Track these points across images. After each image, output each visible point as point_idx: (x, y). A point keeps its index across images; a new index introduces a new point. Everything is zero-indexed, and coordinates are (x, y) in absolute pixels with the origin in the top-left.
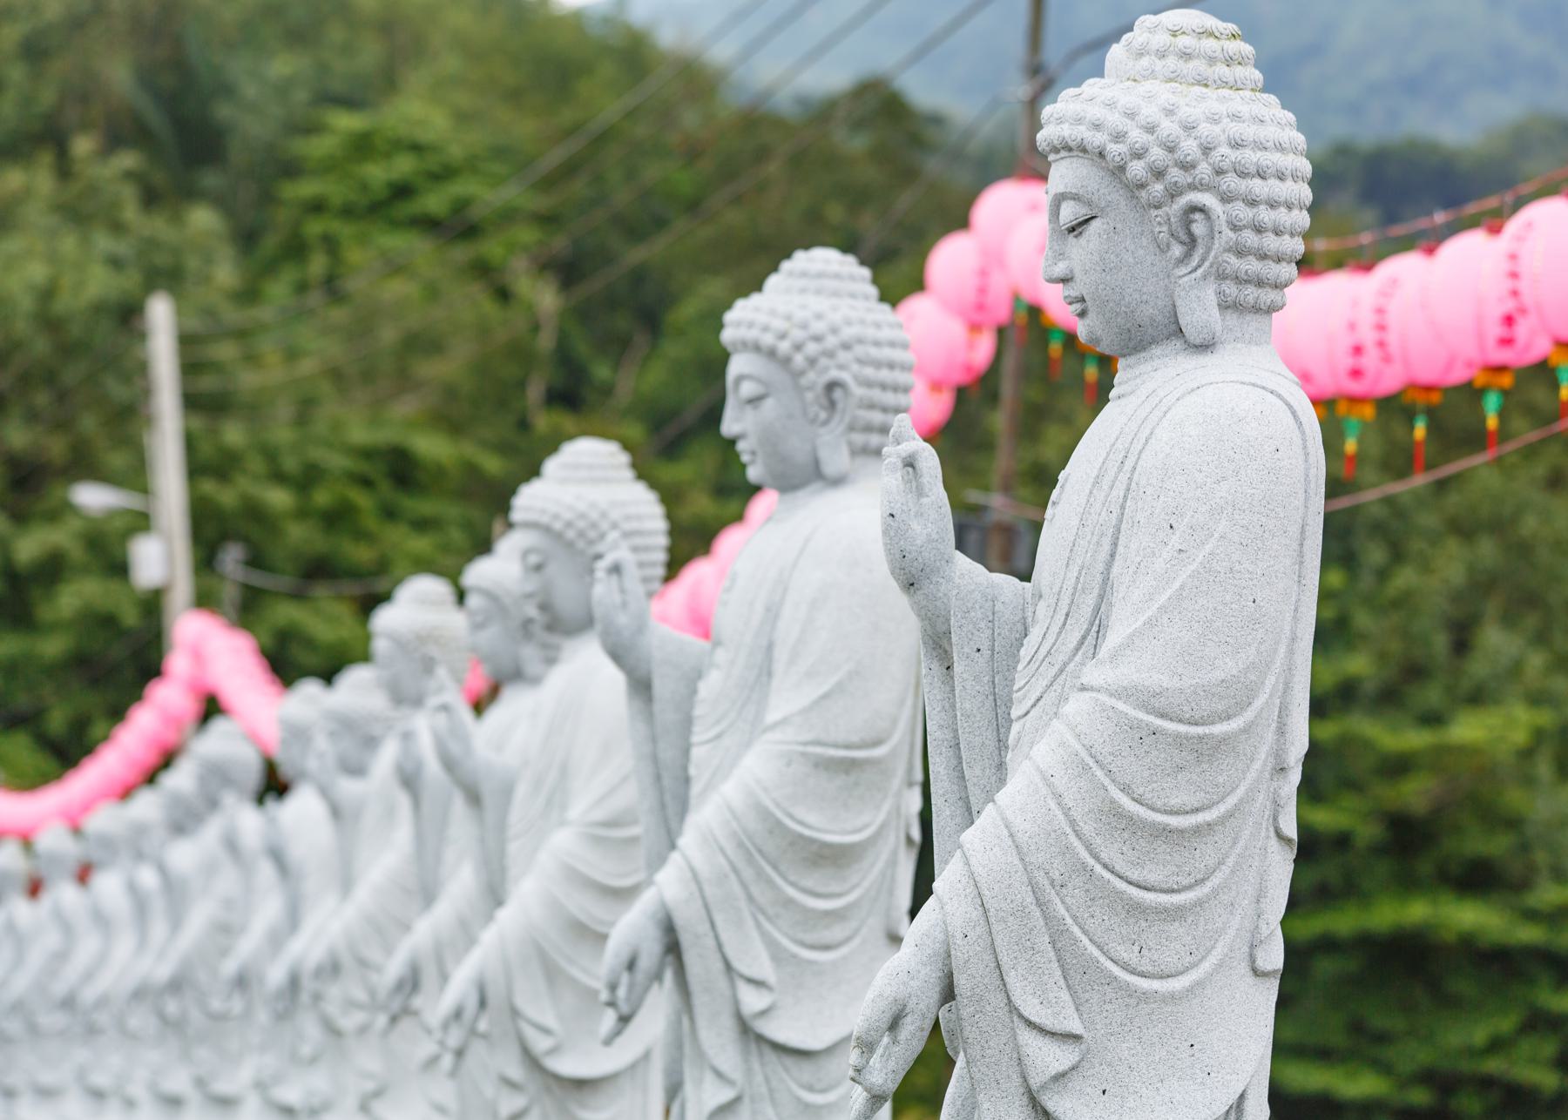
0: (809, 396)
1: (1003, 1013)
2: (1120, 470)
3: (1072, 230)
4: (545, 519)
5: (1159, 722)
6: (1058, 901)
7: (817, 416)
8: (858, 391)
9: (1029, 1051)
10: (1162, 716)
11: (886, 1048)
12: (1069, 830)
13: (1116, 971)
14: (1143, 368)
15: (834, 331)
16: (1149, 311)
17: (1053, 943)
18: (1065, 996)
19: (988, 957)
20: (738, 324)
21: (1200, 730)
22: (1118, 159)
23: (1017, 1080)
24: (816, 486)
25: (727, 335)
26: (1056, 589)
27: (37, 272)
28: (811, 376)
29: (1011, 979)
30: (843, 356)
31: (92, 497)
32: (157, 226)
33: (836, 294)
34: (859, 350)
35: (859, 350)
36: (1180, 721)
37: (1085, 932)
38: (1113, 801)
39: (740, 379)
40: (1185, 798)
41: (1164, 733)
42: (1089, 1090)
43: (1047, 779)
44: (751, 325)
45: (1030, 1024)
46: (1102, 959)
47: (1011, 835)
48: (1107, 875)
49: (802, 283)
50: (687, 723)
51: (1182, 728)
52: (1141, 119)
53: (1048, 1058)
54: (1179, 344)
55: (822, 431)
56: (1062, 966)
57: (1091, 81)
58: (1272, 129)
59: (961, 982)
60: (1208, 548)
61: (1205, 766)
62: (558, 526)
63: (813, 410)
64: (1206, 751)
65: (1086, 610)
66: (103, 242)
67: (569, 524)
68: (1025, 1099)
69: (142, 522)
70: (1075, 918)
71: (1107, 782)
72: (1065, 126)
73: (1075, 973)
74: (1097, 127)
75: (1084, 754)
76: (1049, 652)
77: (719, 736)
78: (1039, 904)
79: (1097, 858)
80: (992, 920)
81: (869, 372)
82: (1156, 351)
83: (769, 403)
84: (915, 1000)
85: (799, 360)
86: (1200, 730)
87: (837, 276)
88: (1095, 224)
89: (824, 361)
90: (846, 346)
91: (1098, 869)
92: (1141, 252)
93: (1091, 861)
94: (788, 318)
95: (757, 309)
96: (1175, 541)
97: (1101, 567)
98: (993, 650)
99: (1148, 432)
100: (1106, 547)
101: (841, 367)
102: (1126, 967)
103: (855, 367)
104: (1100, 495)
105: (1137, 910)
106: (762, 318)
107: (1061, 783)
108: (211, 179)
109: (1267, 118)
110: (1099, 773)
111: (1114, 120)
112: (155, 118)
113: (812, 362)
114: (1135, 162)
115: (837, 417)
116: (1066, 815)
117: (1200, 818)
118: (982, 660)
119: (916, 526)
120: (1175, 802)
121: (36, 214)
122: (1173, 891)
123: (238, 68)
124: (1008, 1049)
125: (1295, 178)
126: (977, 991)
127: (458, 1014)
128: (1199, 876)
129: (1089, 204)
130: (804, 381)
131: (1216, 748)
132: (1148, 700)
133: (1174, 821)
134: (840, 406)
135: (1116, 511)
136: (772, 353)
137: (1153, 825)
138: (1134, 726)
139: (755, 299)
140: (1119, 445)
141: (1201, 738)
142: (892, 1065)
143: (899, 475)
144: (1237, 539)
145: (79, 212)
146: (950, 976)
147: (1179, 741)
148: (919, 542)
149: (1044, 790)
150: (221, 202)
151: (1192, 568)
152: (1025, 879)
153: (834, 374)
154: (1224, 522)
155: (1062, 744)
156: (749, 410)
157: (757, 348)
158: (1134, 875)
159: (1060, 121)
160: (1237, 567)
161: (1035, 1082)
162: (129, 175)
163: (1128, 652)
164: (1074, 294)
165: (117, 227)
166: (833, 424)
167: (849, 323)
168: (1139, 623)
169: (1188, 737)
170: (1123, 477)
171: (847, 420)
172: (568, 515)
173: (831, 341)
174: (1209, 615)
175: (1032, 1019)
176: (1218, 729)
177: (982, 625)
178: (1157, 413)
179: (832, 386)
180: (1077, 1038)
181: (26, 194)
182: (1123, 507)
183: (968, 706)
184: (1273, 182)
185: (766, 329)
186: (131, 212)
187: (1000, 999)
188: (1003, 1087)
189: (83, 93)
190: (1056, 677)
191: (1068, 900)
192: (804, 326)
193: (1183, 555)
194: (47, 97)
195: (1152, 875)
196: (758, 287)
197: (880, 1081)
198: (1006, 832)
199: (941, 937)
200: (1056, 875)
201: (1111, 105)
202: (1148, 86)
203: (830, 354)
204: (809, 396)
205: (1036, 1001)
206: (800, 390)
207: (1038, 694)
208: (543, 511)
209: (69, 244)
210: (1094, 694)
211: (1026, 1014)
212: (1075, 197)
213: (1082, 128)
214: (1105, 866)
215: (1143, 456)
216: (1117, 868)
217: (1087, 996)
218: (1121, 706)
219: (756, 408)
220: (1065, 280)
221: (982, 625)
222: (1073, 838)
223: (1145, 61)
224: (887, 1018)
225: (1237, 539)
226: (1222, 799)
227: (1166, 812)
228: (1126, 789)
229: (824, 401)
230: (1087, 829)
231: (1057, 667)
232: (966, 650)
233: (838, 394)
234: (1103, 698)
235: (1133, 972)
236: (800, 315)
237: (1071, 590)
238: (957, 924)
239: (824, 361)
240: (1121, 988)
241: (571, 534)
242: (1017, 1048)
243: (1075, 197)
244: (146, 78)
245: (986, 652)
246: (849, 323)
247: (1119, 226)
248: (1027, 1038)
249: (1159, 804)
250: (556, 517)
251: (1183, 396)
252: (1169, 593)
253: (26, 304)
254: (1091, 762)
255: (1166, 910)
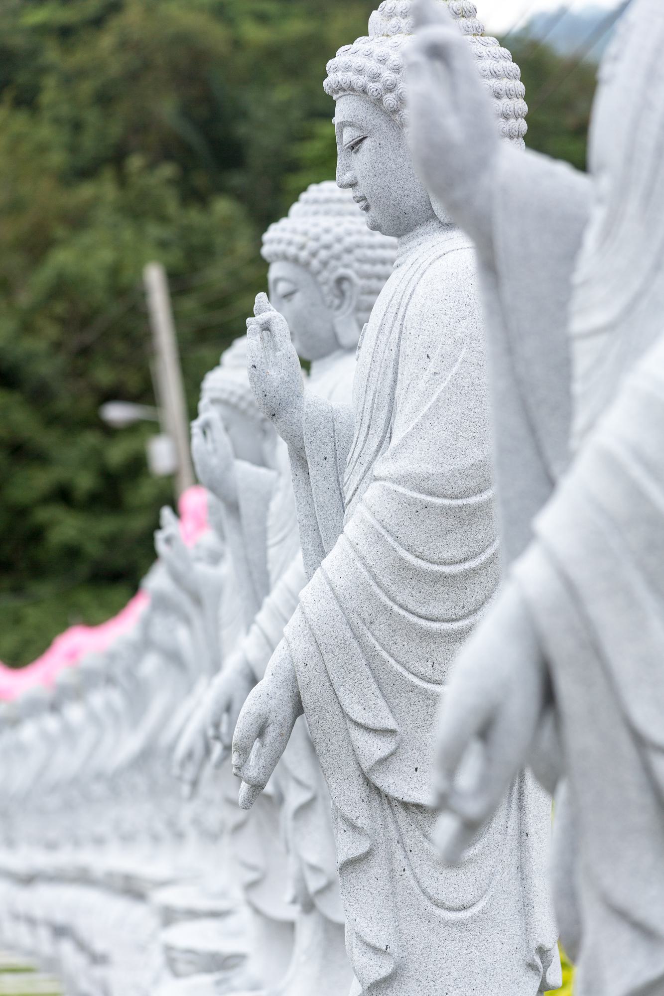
0: (325, 289)
1: (338, 718)
2: (395, 319)
3: (352, 148)
4: (224, 396)
5: (429, 499)
6: (369, 634)
7: (332, 302)
8: (360, 282)
9: (359, 744)
10: (431, 494)
11: (258, 750)
12: (372, 583)
13: (416, 681)
14: (414, 243)
15: (339, 240)
16: (411, 202)
17: (369, 665)
18: (381, 702)
19: (323, 679)
20: (272, 241)
21: (459, 502)
22: (375, 93)
23: (353, 766)
24: (338, 353)
25: (266, 251)
26: (360, 409)
27: (106, 256)
28: (325, 274)
29: (341, 693)
30: (347, 258)
31: (117, 413)
32: (194, 216)
33: (340, 214)
34: (358, 253)
35: (358, 253)
36: (445, 497)
37: (391, 655)
38: (401, 559)
39: (277, 280)
40: (454, 552)
41: (433, 506)
42: (405, 769)
43: (354, 547)
44: (280, 241)
45: (358, 725)
46: (405, 673)
47: (332, 589)
48: (403, 612)
49: (314, 208)
50: (263, 534)
51: (446, 502)
52: (389, 63)
53: (374, 748)
54: (435, 224)
55: (337, 313)
56: (377, 681)
57: (358, 40)
58: (489, 62)
59: (306, 698)
60: (455, 370)
61: (467, 528)
62: (234, 400)
63: (329, 299)
64: (467, 517)
65: (381, 423)
66: (154, 231)
67: (242, 398)
68: (361, 780)
69: (155, 427)
70: (383, 645)
71: (396, 545)
72: (339, 73)
73: (388, 685)
74: (360, 71)
75: (378, 527)
76: (359, 456)
77: (283, 539)
78: (356, 637)
79: (394, 601)
80: (324, 652)
81: (367, 268)
82: (420, 230)
83: (298, 297)
84: (274, 714)
85: (315, 263)
86: (459, 502)
87: (340, 201)
88: (366, 142)
89: (333, 263)
90: (349, 251)
91: (396, 608)
92: (400, 160)
93: (390, 603)
94: (305, 234)
95: (283, 230)
96: (431, 367)
97: (387, 390)
98: (336, 458)
99: (411, 289)
100: (390, 376)
101: (346, 266)
102: (423, 678)
103: (356, 265)
104: (383, 339)
105: (427, 636)
106: (287, 236)
107: (363, 548)
108: (237, 179)
109: (484, 54)
110: (390, 539)
111: (371, 65)
112: (194, 138)
113: (325, 264)
114: (388, 95)
115: (347, 302)
116: (369, 571)
117: (467, 565)
118: (328, 466)
119: (273, 373)
120: (446, 555)
121: (104, 215)
122: (453, 620)
123: (250, 97)
124: (345, 744)
125: (509, 96)
126: (319, 703)
127: (190, 755)
128: (471, 608)
129: (361, 128)
130: (321, 278)
131: (473, 514)
132: (419, 483)
133: (447, 569)
134: (348, 294)
135: (395, 349)
136: (295, 260)
137: (432, 573)
138: (412, 503)
139: (284, 223)
140: (394, 301)
141: (460, 508)
142: (262, 762)
143: (258, 337)
144: (475, 361)
145: (138, 210)
146: (298, 695)
147: (445, 511)
148: (275, 384)
149: (353, 555)
150: (239, 196)
151: (444, 385)
152: (344, 620)
153: (341, 271)
154: (464, 350)
155: (363, 520)
156: (285, 303)
157: (285, 257)
158: (423, 611)
159: (336, 70)
160: (477, 382)
161: (366, 766)
162: (170, 182)
163: (404, 450)
164: (359, 194)
165: (163, 219)
166: (345, 307)
167: (349, 234)
168: (410, 428)
169: (451, 508)
170: (397, 324)
171: (354, 303)
172: (240, 392)
173: (337, 248)
174: (459, 418)
175: (359, 721)
176: (473, 500)
177: (327, 440)
178: (418, 275)
179: (340, 280)
180: (392, 732)
181: (94, 203)
182: (398, 345)
183: (322, 499)
184: (505, 100)
185: (290, 243)
186: (172, 206)
187: (335, 709)
188: (344, 772)
189: (140, 127)
190: (365, 473)
191: (376, 633)
192: (317, 239)
193: (437, 376)
194: (115, 130)
195: (436, 610)
196: (285, 213)
197: (255, 775)
198: (328, 588)
199: (289, 667)
200: (366, 616)
201: (369, 55)
202: (396, 38)
203: (338, 257)
204: (325, 289)
205: (361, 708)
206: (318, 285)
207: (355, 486)
208: (223, 390)
209: (128, 234)
210: (382, 483)
211: (354, 718)
212: (351, 124)
213: (350, 74)
214: (401, 606)
215: (409, 308)
216: (410, 607)
217: (397, 701)
218: (401, 489)
219: (289, 300)
220: (352, 185)
221: (327, 440)
222: (375, 588)
223: (394, 21)
224: (255, 729)
225: (475, 361)
226: (483, 551)
227: (441, 564)
228: (409, 549)
229: (336, 292)
230: (385, 581)
231: (365, 465)
232: (316, 459)
233: (345, 286)
234: (388, 484)
235: (429, 681)
236: (313, 231)
237: (369, 409)
238: (299, 656)
239: (333, 263)
240: (421, 693)
241: (243, 405)
242: (351, 743)
243: (351, 124)
244: (186, 112)
245: (331, 460)
246: (349, 234)
247: (382, 142)
248: (358, 736)
249: (435, 558)
250: (232, 393)
251: (434, 261)
252: (430, 404)
253: (100, 279)
254: (383, 532)
255: (448, 634)
